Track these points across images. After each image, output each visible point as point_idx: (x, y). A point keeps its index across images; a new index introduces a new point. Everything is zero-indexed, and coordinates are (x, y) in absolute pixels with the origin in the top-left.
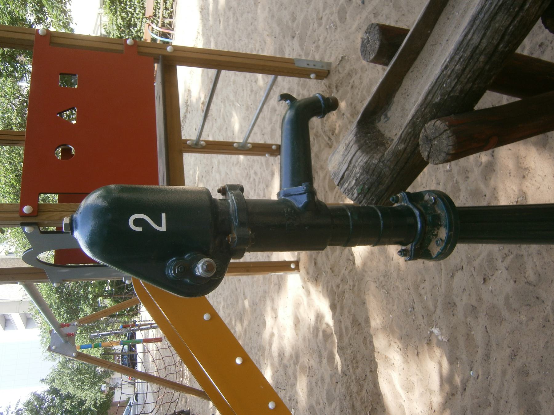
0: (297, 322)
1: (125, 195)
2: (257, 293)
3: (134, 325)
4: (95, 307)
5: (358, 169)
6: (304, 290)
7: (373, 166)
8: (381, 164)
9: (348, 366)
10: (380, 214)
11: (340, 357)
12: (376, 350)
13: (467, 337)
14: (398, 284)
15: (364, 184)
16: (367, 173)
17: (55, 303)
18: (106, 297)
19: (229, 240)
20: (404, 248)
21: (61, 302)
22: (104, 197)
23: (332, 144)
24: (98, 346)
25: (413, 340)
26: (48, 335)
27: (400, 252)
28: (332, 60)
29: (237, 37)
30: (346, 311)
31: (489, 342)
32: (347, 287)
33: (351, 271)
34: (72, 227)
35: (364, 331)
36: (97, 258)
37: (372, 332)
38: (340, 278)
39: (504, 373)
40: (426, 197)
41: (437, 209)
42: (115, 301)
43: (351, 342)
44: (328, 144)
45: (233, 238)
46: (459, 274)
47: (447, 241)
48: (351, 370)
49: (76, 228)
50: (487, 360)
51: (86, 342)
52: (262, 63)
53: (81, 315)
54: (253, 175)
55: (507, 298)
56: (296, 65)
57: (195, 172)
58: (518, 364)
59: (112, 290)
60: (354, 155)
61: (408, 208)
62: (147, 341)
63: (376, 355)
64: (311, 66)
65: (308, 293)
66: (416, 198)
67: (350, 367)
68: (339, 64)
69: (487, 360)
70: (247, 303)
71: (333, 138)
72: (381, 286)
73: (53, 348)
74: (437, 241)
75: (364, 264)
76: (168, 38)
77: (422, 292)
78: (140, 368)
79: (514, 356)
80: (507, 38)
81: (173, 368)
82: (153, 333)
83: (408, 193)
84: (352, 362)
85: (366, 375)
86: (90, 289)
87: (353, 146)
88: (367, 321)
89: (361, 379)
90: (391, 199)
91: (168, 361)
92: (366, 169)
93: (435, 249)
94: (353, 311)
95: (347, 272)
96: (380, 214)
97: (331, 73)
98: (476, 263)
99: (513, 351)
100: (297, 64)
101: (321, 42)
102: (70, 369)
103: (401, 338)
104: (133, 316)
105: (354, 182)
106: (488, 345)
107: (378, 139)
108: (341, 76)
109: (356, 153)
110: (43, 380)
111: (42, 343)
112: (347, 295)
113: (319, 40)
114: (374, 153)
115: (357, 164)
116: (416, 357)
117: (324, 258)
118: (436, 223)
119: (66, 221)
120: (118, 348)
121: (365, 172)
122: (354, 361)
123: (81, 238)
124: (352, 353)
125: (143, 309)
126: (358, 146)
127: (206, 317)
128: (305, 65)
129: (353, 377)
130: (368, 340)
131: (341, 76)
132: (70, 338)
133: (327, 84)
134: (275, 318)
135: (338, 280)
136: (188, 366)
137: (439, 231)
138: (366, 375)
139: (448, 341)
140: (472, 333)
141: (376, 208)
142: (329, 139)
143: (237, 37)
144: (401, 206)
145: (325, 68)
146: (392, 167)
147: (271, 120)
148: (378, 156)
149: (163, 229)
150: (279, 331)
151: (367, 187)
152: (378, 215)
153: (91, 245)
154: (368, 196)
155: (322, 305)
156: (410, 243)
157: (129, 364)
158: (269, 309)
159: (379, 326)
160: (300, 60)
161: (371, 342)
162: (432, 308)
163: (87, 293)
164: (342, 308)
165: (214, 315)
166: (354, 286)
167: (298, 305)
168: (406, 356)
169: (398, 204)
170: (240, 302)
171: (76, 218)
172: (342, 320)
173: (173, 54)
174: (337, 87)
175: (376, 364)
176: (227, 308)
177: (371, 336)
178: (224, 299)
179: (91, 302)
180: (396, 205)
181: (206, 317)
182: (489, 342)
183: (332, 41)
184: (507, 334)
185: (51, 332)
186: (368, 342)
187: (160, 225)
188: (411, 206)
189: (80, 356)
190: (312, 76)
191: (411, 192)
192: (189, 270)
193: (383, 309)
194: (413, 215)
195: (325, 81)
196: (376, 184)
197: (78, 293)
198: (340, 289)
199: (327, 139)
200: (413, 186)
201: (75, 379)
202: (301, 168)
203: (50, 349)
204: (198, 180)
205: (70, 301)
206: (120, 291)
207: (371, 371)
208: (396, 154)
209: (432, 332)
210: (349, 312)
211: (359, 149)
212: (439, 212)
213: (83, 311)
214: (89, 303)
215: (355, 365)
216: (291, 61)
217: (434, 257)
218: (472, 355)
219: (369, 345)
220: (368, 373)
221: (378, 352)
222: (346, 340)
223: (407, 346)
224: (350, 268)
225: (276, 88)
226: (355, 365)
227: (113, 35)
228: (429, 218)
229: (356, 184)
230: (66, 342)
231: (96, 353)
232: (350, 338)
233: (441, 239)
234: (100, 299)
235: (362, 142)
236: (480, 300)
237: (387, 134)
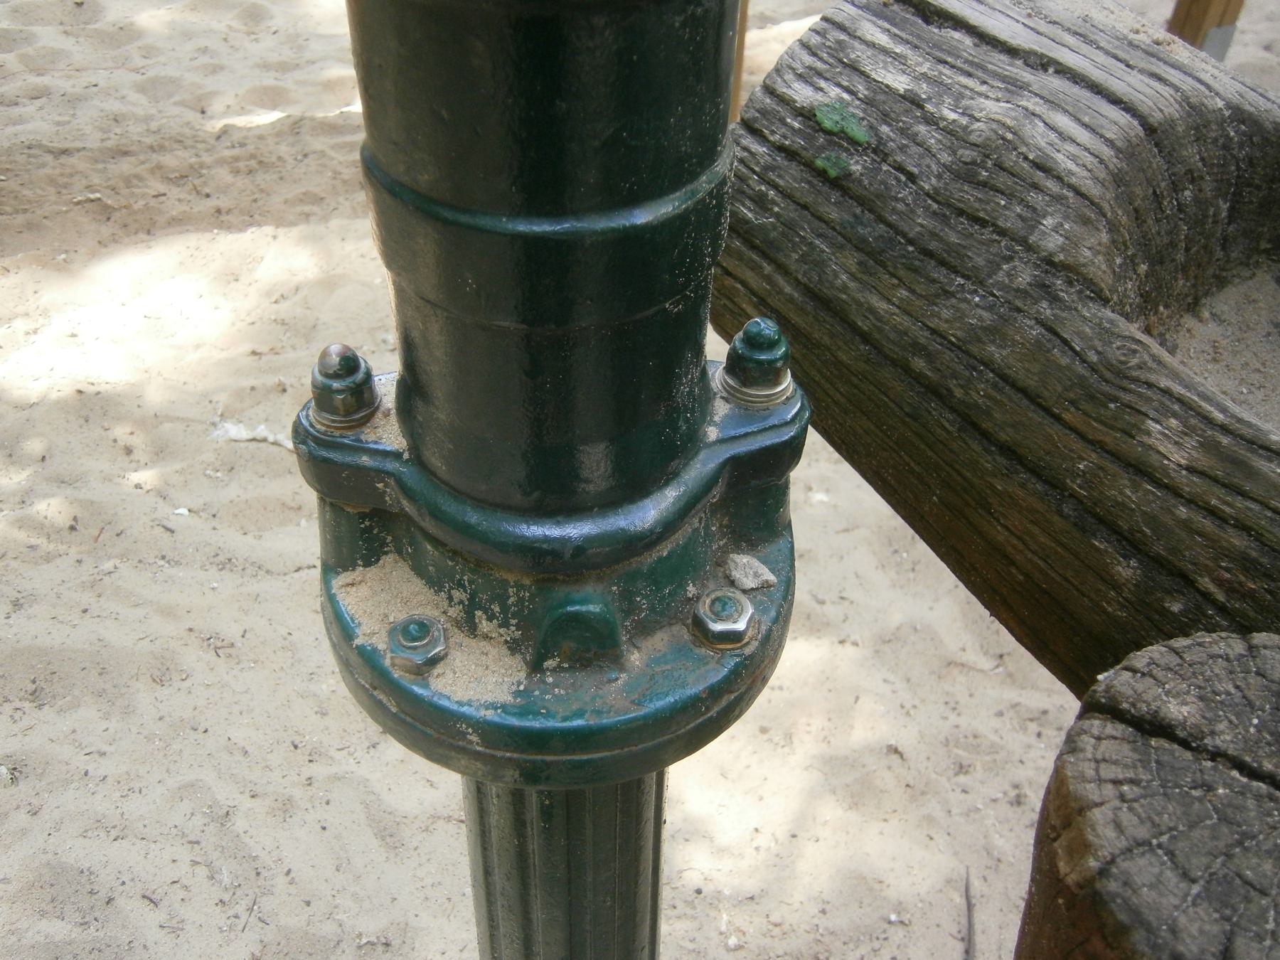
5: (992, 107)
7: (1010, 218)
8: (1024, 278)
9: (242, 145)
10: (643, 216)
12: (281, 231)
13: (293, 504)
15: (879, 151)
16: (966, 174)
27: (350, 364)
31: (268, 572)
35: (341, 199)
39: (168, 612)
40: (749, 569)
41: (659, 641)
43: (311, 156)
47: (416, 700)
50: (217, 560)
58: (194, 658)
60: (1097, 89)
61: (690, 443)
63: (269, 230)
66: (753, 498)
67: (236, 152)
69: (217, 560)
74: (424, 628)
79: (218, 646)
83: (791, 451)
84: (253, 156)
85: (208, 196)
87: (1166, 91)
89: (197, 182)
90: (767, 327)
92: (994, 170)
96: (643, 216)
99: (232, 645)
105: (900, 82)
107: (1184, 269)
109: (1115, 101)
114: (1113, 228)
115: (1032, 103)
118: (561, 642)
121: (967, 154)
122: (253, 163)
124: (280, 158)
126: (1171, 123)
129: (207, 159)
130: (315, 209)
137: (496, 652)
138: (208, 196)
140: (303, 522)
141: (704, 184)
144: (706, 397)
146: (995, 352)
148: (1092, 252)
151: (856, 168)
152: (634, 200)
154: (791, 177)
156: (415, 447)
169: (717, 377)
175: (242, 228)
180: (715, 347)
182: (268, 572)
184: (284, 631)
186: (307, 209)
188: (700, 468)
191: (798, 475)
194: (633, 487)
196: (871, 232)
200: (1018, 801)
207: (219, 211)
208: (1110, 396)
211: (1150, 130)
212: (635, 659)
215: (241, 165)
217: (338, 582)
218: (235, 516)
219: (299, 209)
220: (212, 203)
221: (275, 237)
222: (319, 143)
223: (283, 323)
226: (241, 165)
228: (591, 601)
229: (880, 102)
232: (323, 154)
233: (433, 662)
235: (1191, 154)
237: (1199, 333)
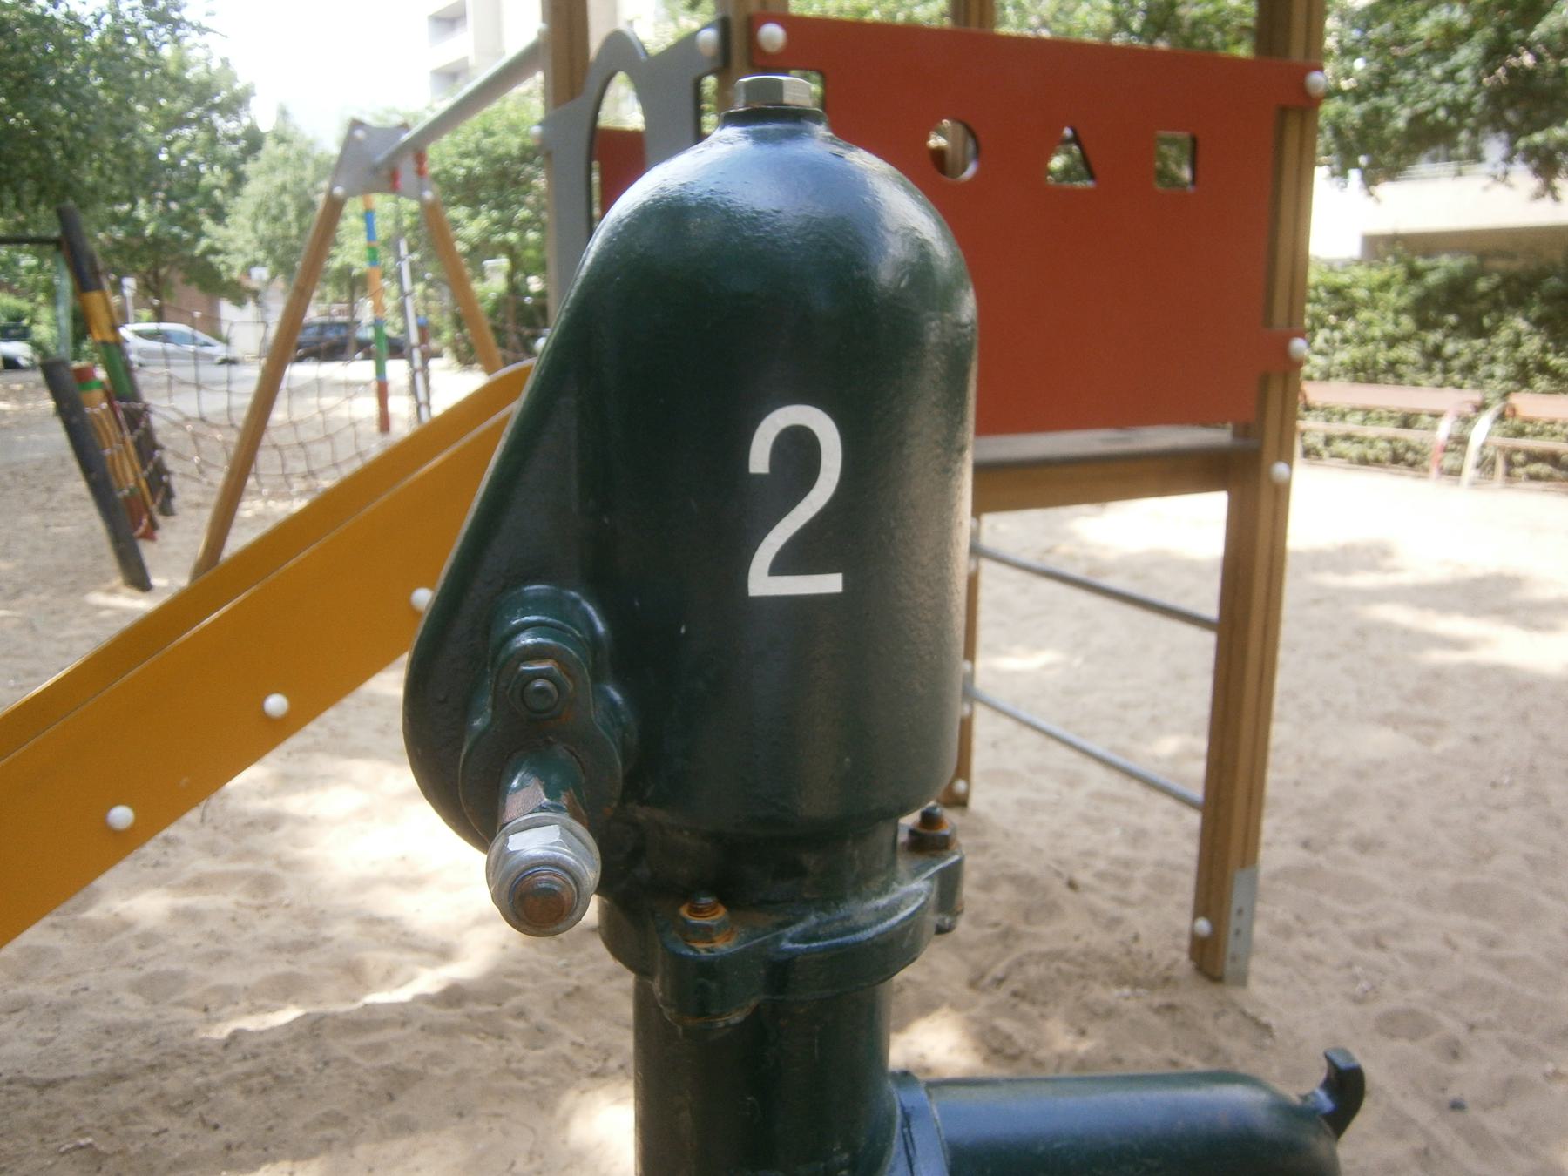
3: (428, 356)
4: (482, 250)
9: (255, 1056)
11: (289, 1025)
17: (495, 144)
18: (510, 277)
19: (696, 911)
21: (499, 160)
22: (921, 268)
23: (984, 990)
24: (373, 258)
26: (396, 120)
28: (1256, 989)
30: (437, 1045)
32: (516, 1047)
33: (569, 1062)
34: (765, 115)
36: (608, 241)
38: (548, 1022)
42: (500, 303)
44: (982, 976)
45: (706, 933)
48: (238, 1068)
49: (760, 138)
51: (383, 228)
53: (459, 213)
59: (528, 294)
62: (382, 392)
64: (1234, 922)
67: (249, 1065)
68: (1244, 1014)
71: (1002, 994)
73: (359, 134)
78: (300, 372)
81: (301, 467)
82: (401, 408)
84: (268, 1070)
91: (323, 452)
94: (437, 1071)
95: (565, 1048)
97: (1213, 989)
100: (1240, 878)
101: (1313, 946)
102: (313, 185)
104: (456, 351)
108: (1208, 1023)
110: (284, 113)
111: (388, 112)
112: (489, 1047)
113: (1309, 935)
120: (366, 311)
123: (710, 164)
124: (299, 1071)
125: (474, 380)
128: (1238, 899)
129: (215, 1078)
131: (1208, 1023)
132: (389, 180)
133: (1175, 973)
135: (539, 1015)
136: (303, 514)
142: (1000, 981)
145: (1229, 967)
149: (762, 582)
153: (669, 214)
157: (297, 343)
163: (524, 225)
164: (448, 1031)
166: (520, 1075)
171: (811, 135)
172: (408, 1030)
174: (1171, 1008)
179: (498, 238)
183: (1314, 983)
185: (405, 127)
187: (784, 564)
189: (335, 208)
190: (1203, 926)
195: (1183, 960)
197: (521, 204)
198: (510, 1022)
199: (998, 970)
201: (286, 199)
203: (356, 124)
205: (496, 182)
206: (519, 315)
210: (435, 1059)
213: (472, 217)
214: (496, 233)
216: (1249, 856)
222: (341, 1047)
224: (581, 1060)
225: (1167, 812)
230: (375, 170)
231: (350, 251)
232: (346, 1061)
234: (503, 262)
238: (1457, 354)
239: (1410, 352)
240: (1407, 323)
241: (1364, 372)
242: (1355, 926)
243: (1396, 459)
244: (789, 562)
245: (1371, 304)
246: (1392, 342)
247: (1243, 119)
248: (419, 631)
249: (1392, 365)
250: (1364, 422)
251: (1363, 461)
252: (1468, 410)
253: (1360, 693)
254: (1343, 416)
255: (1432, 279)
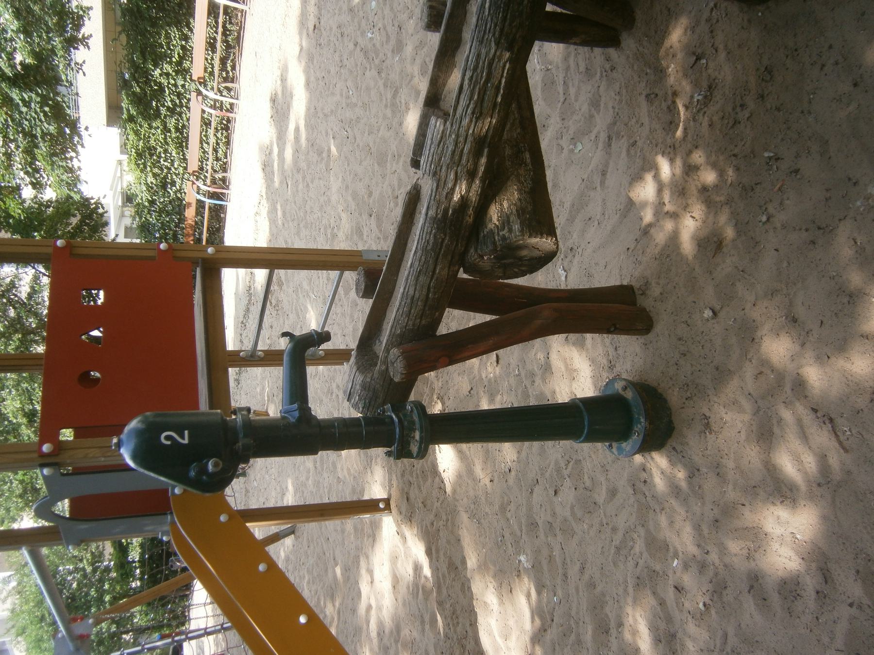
0: (396, 581)
1: (158, 419)
2: (349, 552)
5: (358, 387)
6: (399, 537)
14: (487, 510)
20: (389, 449)
22: (142, 422)
25: (505, 576)
29: (308, 208)
32: (441, 523)
34: (119, 445)
37: (469, 575)
46: (537, 489)
52: (323, 258)
54: (335, 390)
55: (572, 507)
56: (364, 258)
57: (263, 389)
58: (586, 577)
65: (404, 539)
70: (338, 570)
72: (472, 516)
75: (454, 491)
76: (222, 200)
77: (509, 515)
79: (582, 569)
80: (432, 290)
86: (107, 587)
88: (464, 562)
92: (364, 386)
93: (414, 449)
98: (547, 475)
103: (494, 576)
106: (564, 563)
116: (510, 595)
117: (417, 492)
119: (115, 440)
127: (262, 567)
134: (372, 582)
139: (533, 567)
143: (308, 208)
147: (352, 316)
149: (186, 441)
150: (377, 600)
153: (134, 458)
154: (371, 409)
155: (418, 550)
158: (363, 572)
159: (475, 566)
160: (368, 251)
161: (469, 588)
162: (519, 534)
163: (101, 593)
164: (437, 551)
165: (272, 565)
167: (394, 559)
168: (500, 597)
170: (330, 571)
173: (217, 256)
176: (313, 583)
177: (469, 580)
178: (308, 571)
181: (262, 567)
187: (183, 438)
192: (203, 470)
193: (477, 544)
197: (87, 594)
202: (297, 389)
204: (268, 400)
209: (520, 561)
227: (142, 199)
229: (360, 399)
236: (554, 514)
238: (172, 101)
239: (171, 123)
240: (157, 123)
241: (182, 143)
242: (392, 204)
243: (227, 128)
244: (183, 438)
245: (147, 139)
246: (166, 129)
247: (64, 237)
248: (194, 491)
249: (177, 129)
250: (208, 143)
251: (228, 143)
252: (200, 98)
253: (320, 179)
254: (204, 152)
255: (133, 112)
